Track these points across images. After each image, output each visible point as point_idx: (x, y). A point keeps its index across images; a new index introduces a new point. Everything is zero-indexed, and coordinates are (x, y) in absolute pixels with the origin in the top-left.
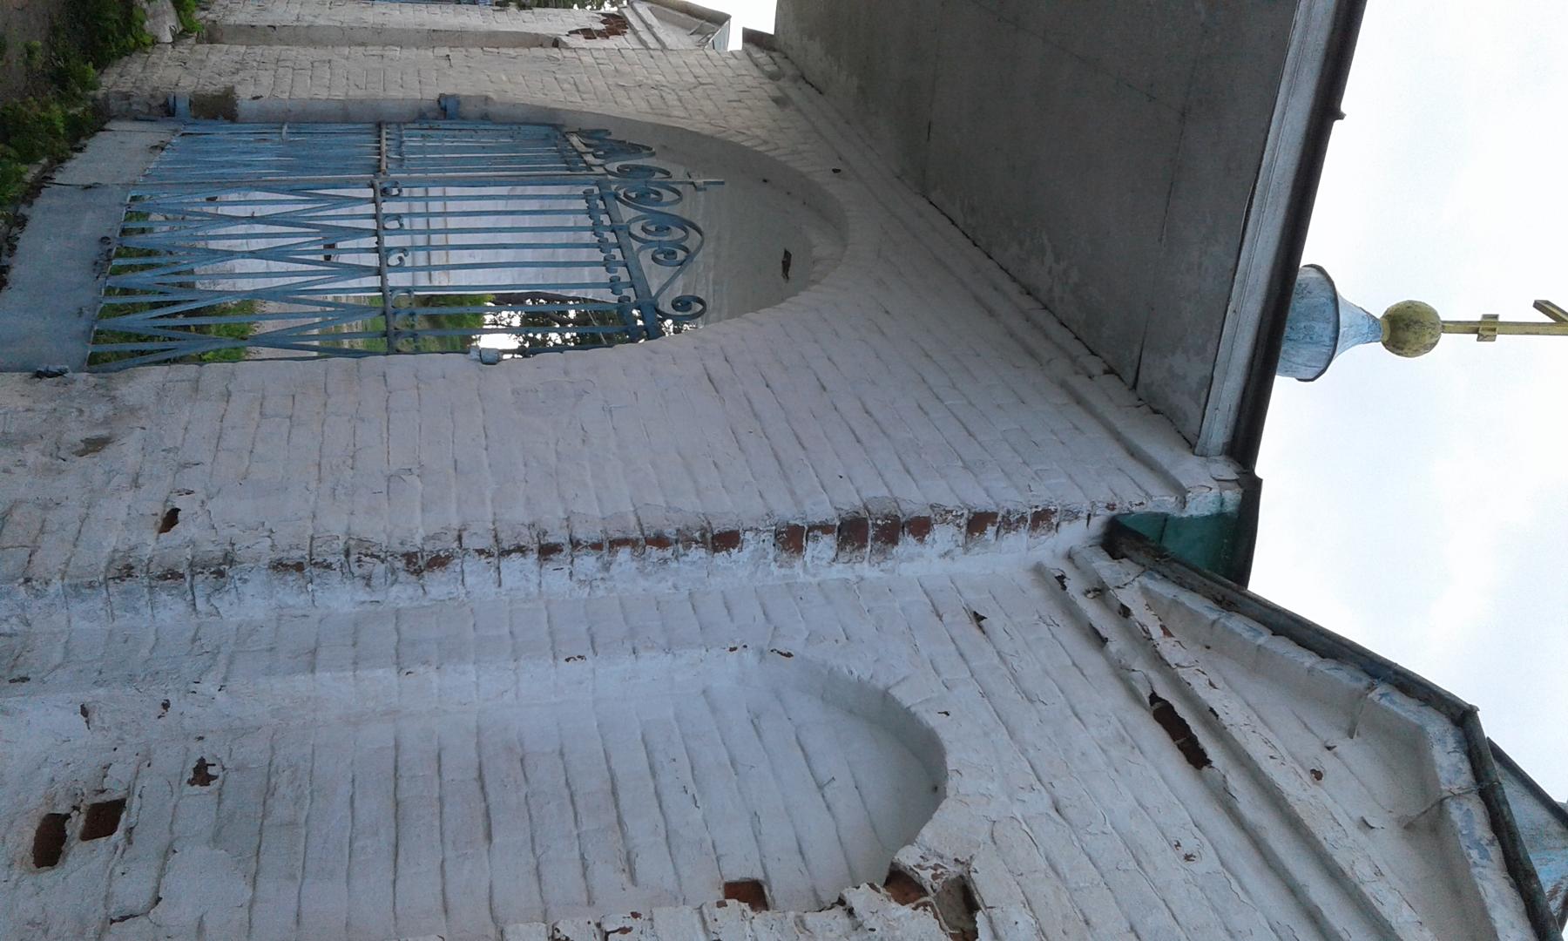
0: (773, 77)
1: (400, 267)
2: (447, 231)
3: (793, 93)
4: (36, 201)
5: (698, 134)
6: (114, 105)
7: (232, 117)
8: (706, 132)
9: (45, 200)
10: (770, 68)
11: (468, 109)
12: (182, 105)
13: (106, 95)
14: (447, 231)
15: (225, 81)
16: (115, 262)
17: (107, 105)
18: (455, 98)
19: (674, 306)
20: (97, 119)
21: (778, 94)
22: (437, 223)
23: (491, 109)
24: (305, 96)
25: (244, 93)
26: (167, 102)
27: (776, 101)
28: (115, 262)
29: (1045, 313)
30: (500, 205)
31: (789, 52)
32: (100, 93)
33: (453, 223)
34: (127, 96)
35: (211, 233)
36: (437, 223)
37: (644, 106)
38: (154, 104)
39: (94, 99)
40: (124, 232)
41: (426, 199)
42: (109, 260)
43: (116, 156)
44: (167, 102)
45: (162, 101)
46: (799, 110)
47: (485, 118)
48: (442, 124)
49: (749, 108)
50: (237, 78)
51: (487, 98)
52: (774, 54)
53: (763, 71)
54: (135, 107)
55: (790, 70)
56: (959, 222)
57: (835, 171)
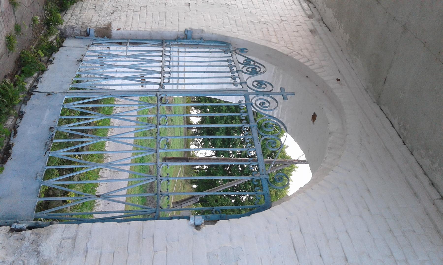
0: (310, 17)
1: (168, 83)
2: (184, 78)
3: (319, 29)
4: (29, 102)
5: (281, 53)
6: (69, 31)
7: (109, 36)
8: (285, 53)
9: (33, 101)
10: (309, 12)
11: (196, 35)
12: (92, 32)
13: (65, 27)
14: (184, 78)
15: (108, 19)
16: (54, 141)
17: (65, 31)
18: (191, 31)
19: (260, 104)
20: (63, 37)
21: (312, 27)
22: (181, 75)
23: (204, 35)
24: (136, 29)
25: (114, 27)
26: (86, 31)
27: (311, 31)
28: (54, 141)
29: (433, 188)
30: (205, 69)
31: (317, 6)
32: (62, 26)
33: (187, 75)
34: (72, 27)
35: (105, 71)
36: (181, 75)
37: (261, 35)
38: (82, 31)
39: (61, 29)
40: (60, 123)
41: (178, 78)
42: (52, 140)
43: (72, 48)
44: (86, 31)
45: (85, 30)
46: (321, 38)
47: (201, 39)
48: (185, 42)
49: (301, 36)
50: (113, 17)
51: (202, 31)
52: (310, 5)
53: (306, 13)
54: (75, 32)
55: (318, 17)
56: (396, 125)
57: (338, 80)
